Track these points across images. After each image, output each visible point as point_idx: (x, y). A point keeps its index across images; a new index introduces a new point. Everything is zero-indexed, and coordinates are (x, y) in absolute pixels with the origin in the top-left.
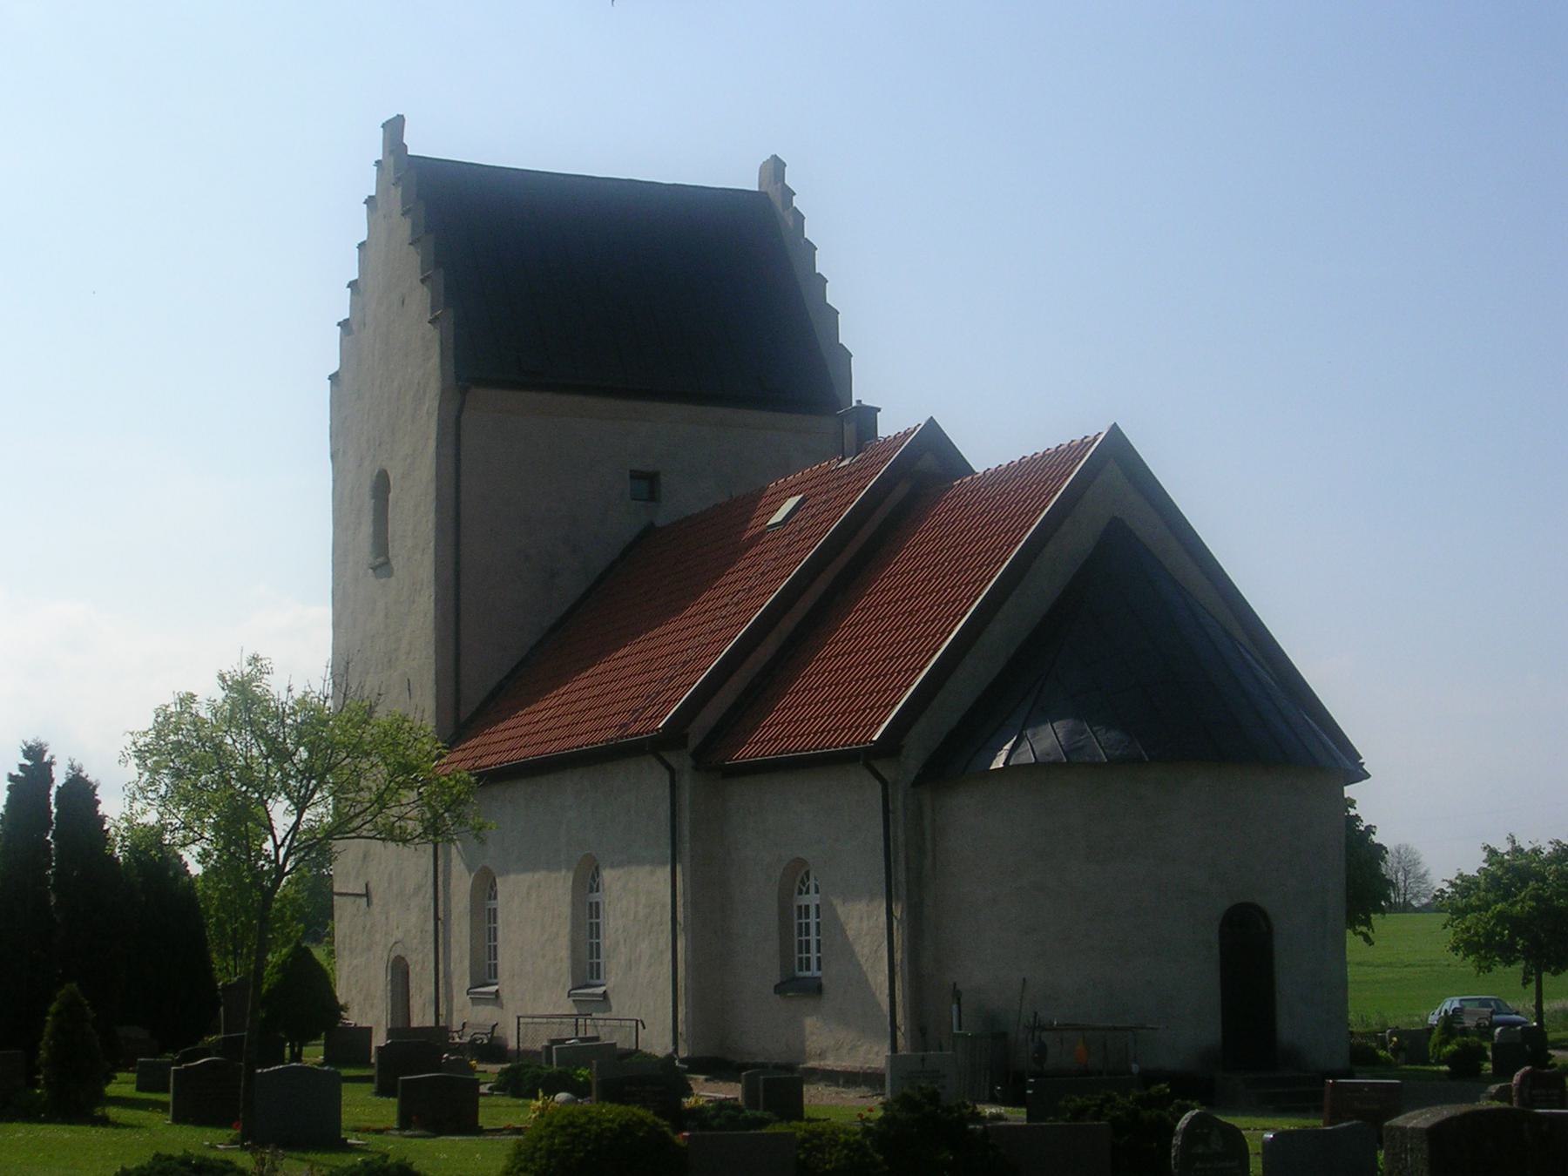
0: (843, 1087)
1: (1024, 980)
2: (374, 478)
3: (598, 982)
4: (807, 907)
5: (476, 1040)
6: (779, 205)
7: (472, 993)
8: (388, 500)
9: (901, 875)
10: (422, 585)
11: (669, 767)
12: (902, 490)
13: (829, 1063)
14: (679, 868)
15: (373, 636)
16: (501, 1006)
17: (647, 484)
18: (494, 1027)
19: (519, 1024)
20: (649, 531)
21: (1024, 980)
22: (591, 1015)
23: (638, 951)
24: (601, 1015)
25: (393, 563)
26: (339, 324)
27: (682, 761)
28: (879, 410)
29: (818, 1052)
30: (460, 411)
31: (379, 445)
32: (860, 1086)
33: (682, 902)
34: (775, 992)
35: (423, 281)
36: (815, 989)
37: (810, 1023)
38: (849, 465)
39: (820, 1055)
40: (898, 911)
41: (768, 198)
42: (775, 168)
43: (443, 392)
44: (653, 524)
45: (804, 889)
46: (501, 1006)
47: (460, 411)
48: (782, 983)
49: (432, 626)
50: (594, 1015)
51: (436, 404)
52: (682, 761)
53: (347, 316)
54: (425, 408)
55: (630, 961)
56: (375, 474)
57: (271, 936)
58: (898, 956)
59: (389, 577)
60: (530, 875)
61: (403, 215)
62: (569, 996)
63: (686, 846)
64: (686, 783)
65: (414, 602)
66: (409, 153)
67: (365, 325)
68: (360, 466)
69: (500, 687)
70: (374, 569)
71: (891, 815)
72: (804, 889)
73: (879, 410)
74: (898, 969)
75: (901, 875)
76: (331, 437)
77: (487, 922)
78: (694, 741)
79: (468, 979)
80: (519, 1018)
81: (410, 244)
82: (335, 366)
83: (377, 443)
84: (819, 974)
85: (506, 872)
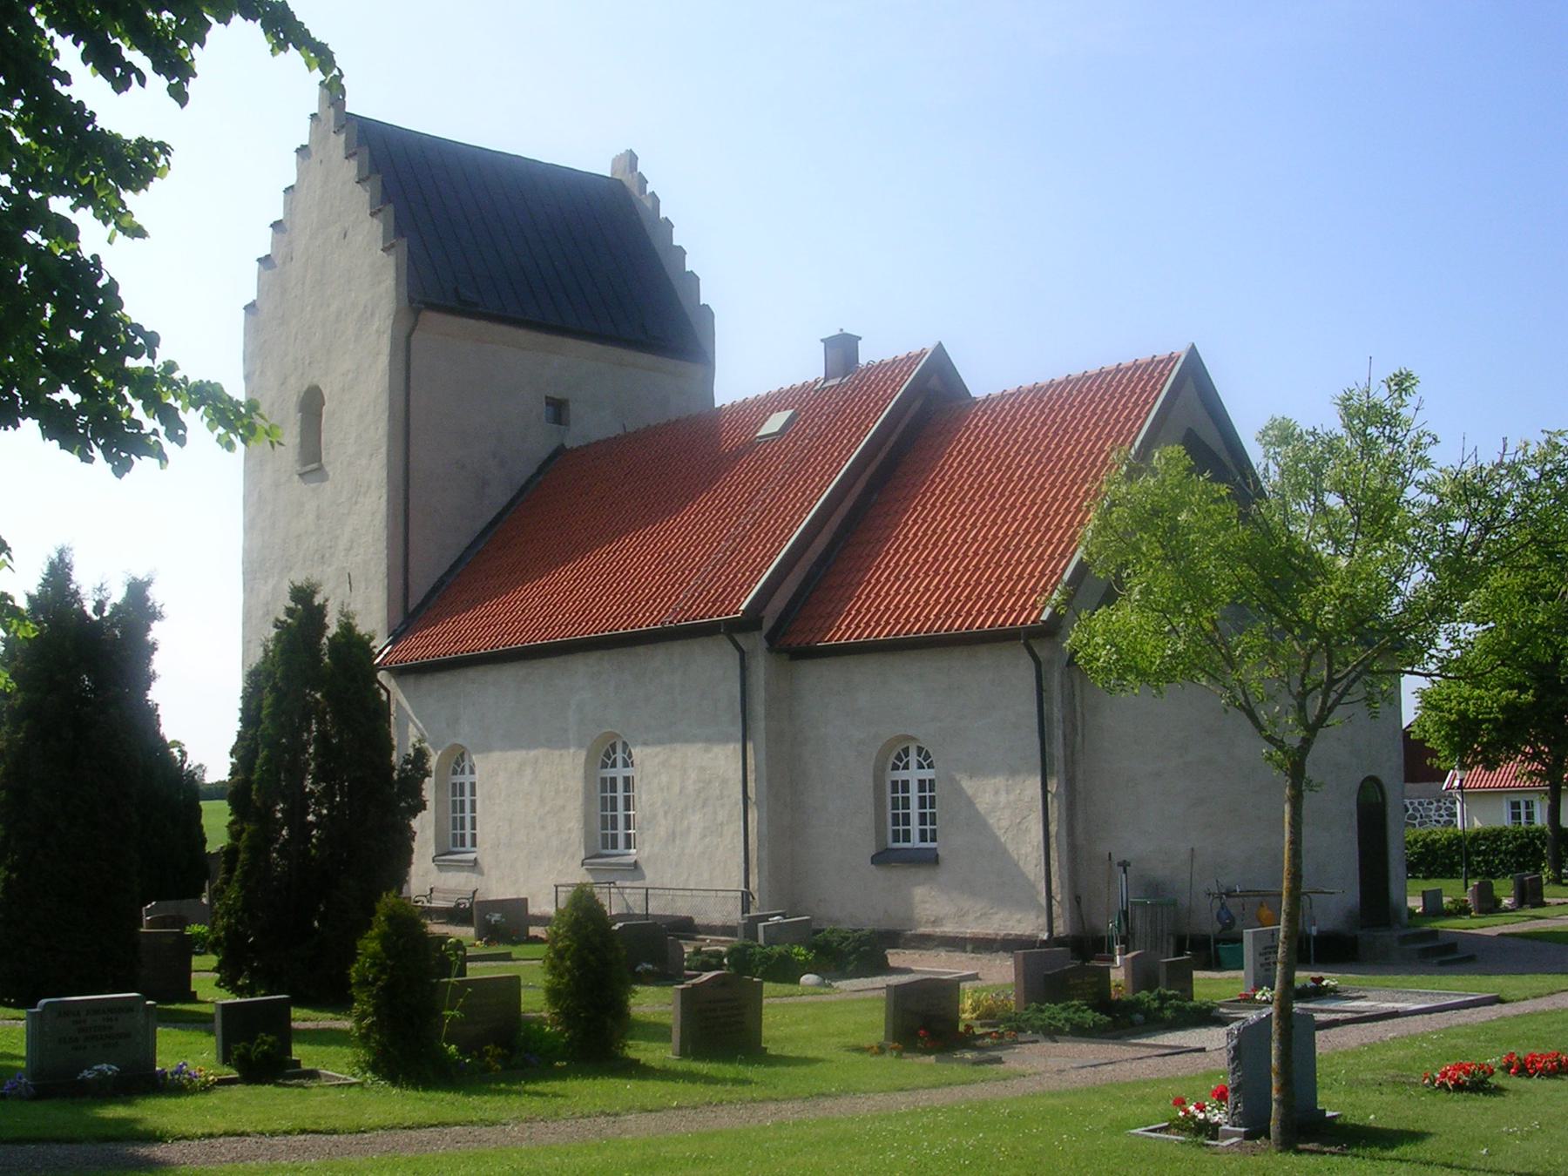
0: (973, 952)
1: (1192, 850)
2: (302, 394)
3: (614, 852)
4: (462, 785)
5: (459, 904)
6: (635, 190)
7: (588, 864)
8: (321, 415)
9: (1057, 750)
10: (369, 487)
11: (742, 653)
12: (917, 405)
13: (946, 929)
14: (750, 746)
15: (299, 536)
16: (482, 873)
17: (558, 410)
18: (474, 892)
19: (557, 892)
20: (560, 452)
21: (1192, 850)
22: (614, 883)
23: (686, 823)
24: (628, 884)
25: (328, 469)
26: (259, 260)
27: (755, 643)
28: (860, 338)
29: (933, 919)
30: (412, 330)
31: (310, 364)
32: (997, 951)
33: (753, 777)
34: (872, 863)
35: (372, 214)
36: (929, 860)
37: (919, 892)
38: (839, 385)
39: (934, 922)
40: (1053, 786)
41: (624, 185)
42: (631, 159)
43: (397, 312)
44: (563, 445)
45: (459, 770)
46: (482, 873)
47: (412, 330)
48: (878, 854)
49: (384, 523)
50: (618, 883)
51: (389, 322)
52: (755, 643)
53: (268, 252)
54: (374, 328)
55: (674, 833)
56: (304, 389)
57: (403, 804)
58: (1053, 828)
59: (323, 481)
60: (524, 752)
61: (346, 158)
62: (583, 864)
63: (760, 725)
64: (761, 666)
65: (356, 503)
66: (347, 110)
67: (292, 259)
68: (283, 384)
69: (441, 581)
70: (301, 475)
71: (1044, 694)
72: (459, 770)
73: (860, 338)
74: (1053, 840)
75: (1057, 750)
76: (244, 360)
77: (450, 794)
78: (768, 624)
79: (433, 847)
80: (556, 887)
81: (358, 182)
82: (251, 295)
83: (307, 362)
84: (933, 845)
85: (487, 748)
